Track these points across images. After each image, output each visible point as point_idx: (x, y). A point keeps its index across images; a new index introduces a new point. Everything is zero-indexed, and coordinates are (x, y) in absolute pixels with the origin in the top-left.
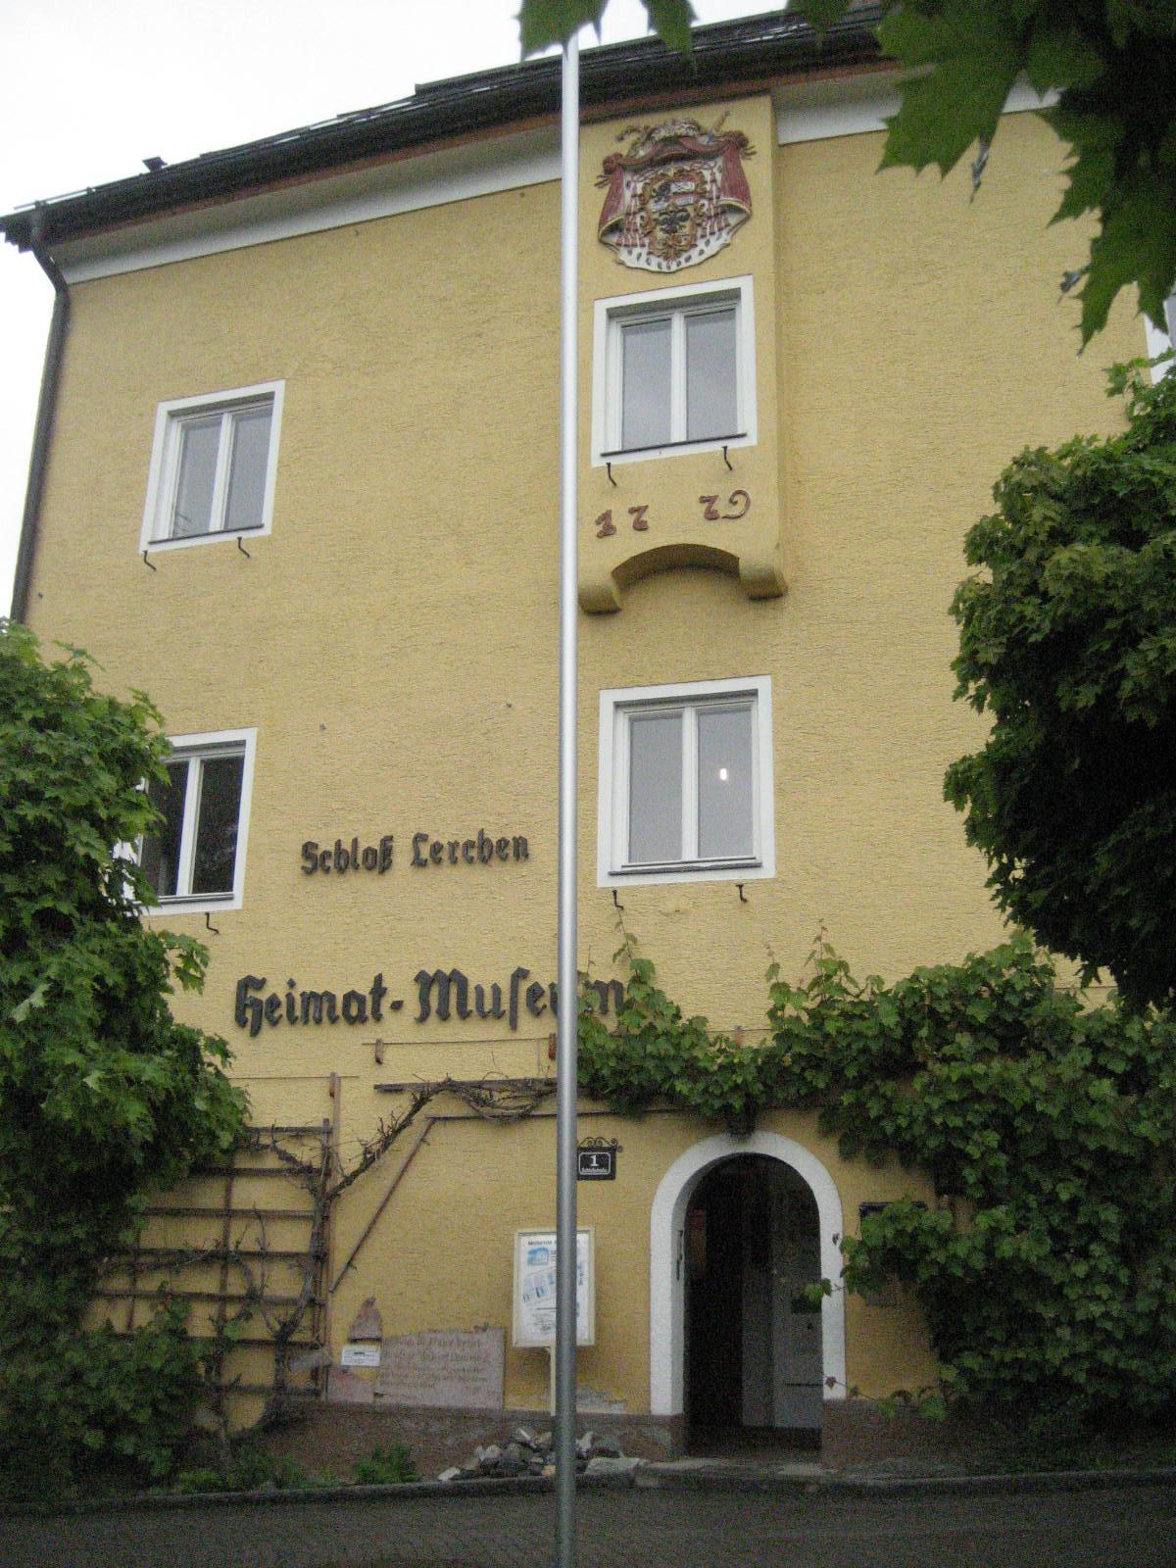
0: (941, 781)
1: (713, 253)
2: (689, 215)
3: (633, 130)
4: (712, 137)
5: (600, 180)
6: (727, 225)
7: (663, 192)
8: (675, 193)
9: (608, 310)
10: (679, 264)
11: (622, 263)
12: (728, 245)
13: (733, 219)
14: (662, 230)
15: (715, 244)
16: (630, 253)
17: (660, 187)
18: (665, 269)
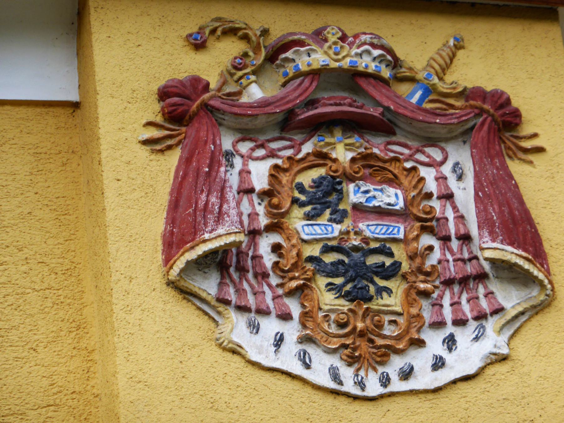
0: (524, 114)
1: (471, 371)
2: (397, 265)
3: (231, 31)
4: (429, 90)
5: (154, 133)
6: (498, 311)
7: (325, 198)
8: (356, 207)
9: (401, 379)
10: (385, 381)
11: (235, 351)
12: (504, 359)
13: (511, 299)
14: (330, 287)
15: (469, 353)
16: (255, 328)
17: (318, 183)
18: (349, 387)
